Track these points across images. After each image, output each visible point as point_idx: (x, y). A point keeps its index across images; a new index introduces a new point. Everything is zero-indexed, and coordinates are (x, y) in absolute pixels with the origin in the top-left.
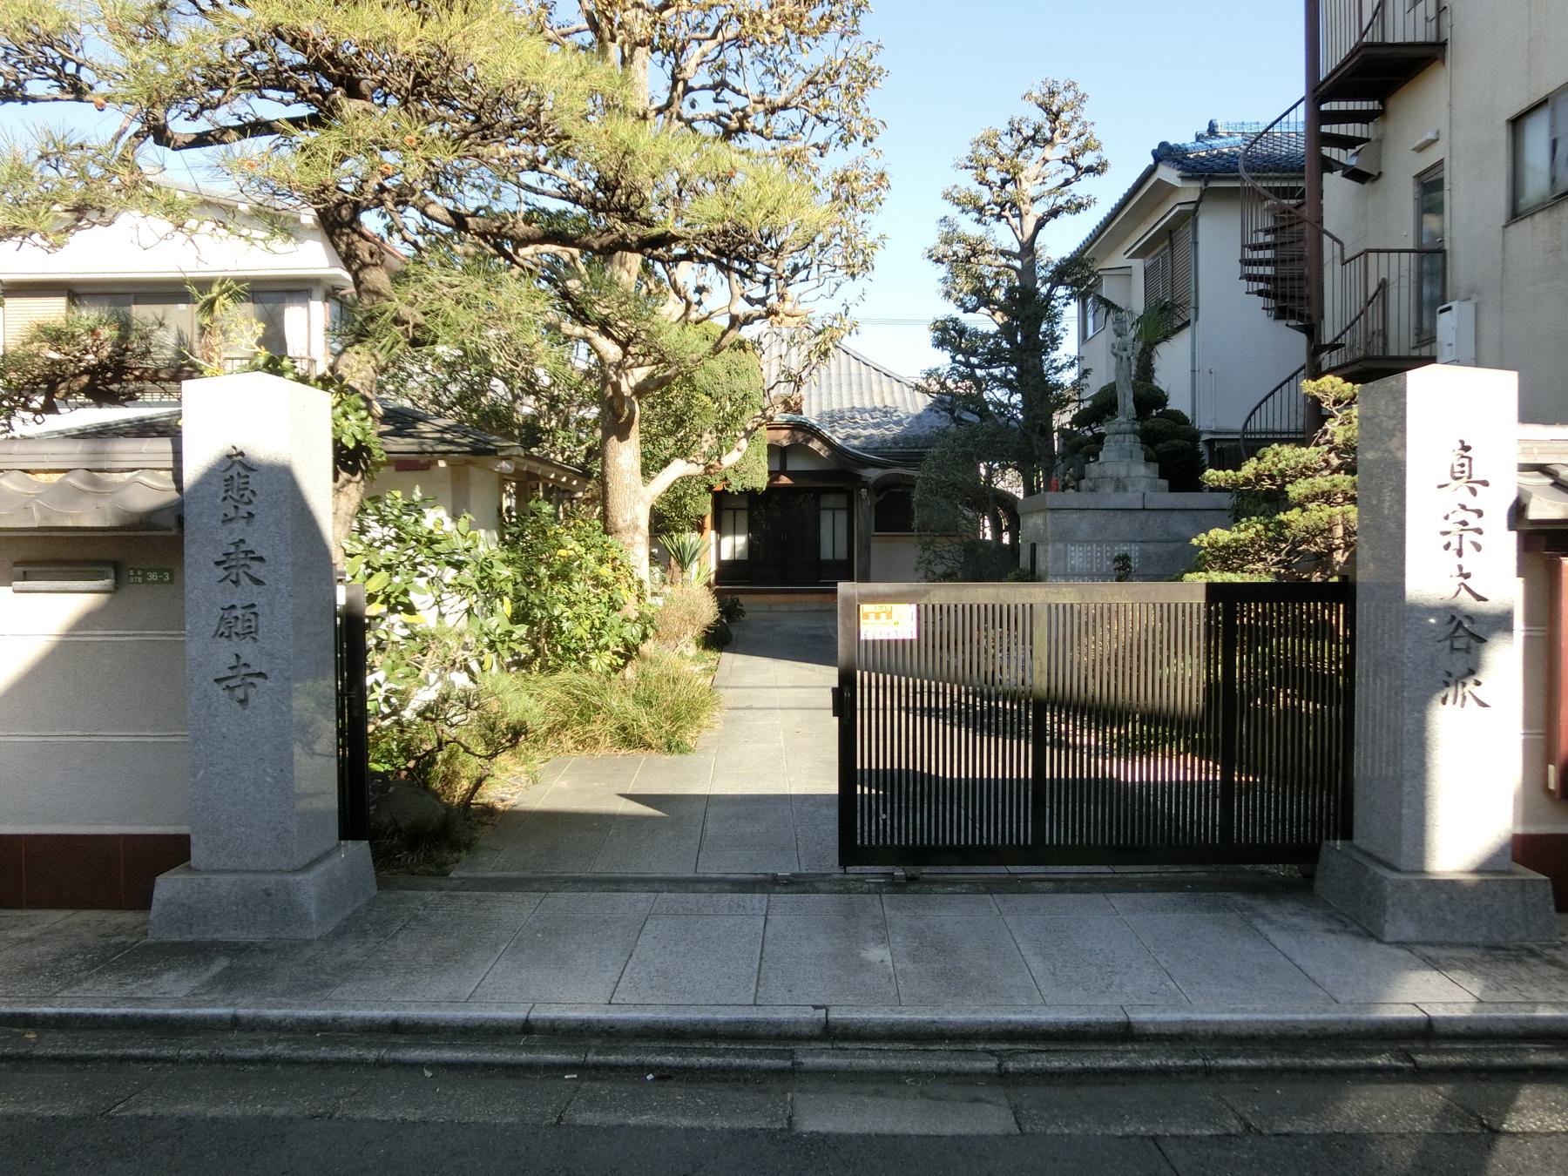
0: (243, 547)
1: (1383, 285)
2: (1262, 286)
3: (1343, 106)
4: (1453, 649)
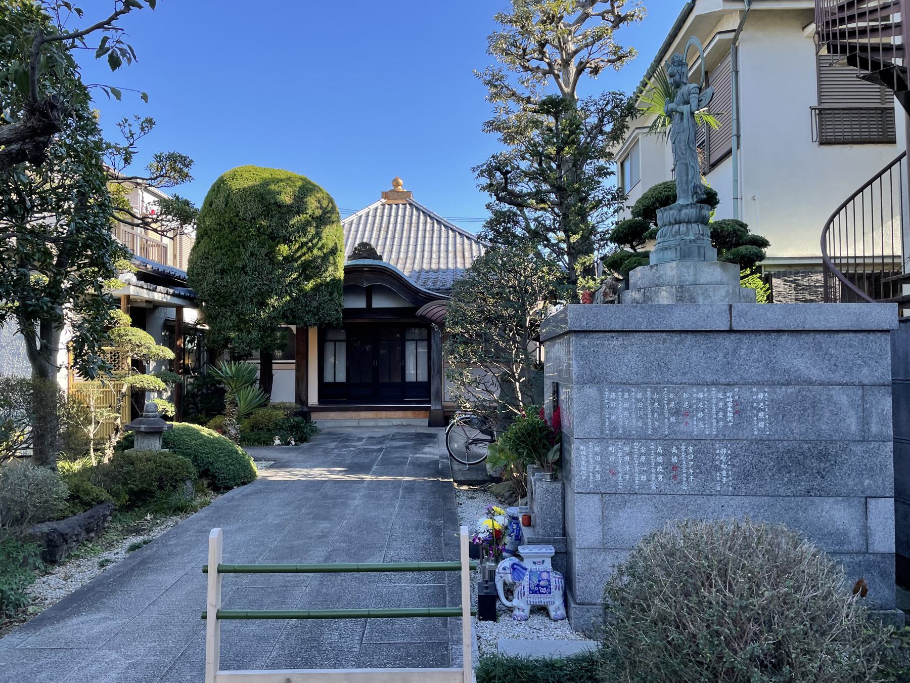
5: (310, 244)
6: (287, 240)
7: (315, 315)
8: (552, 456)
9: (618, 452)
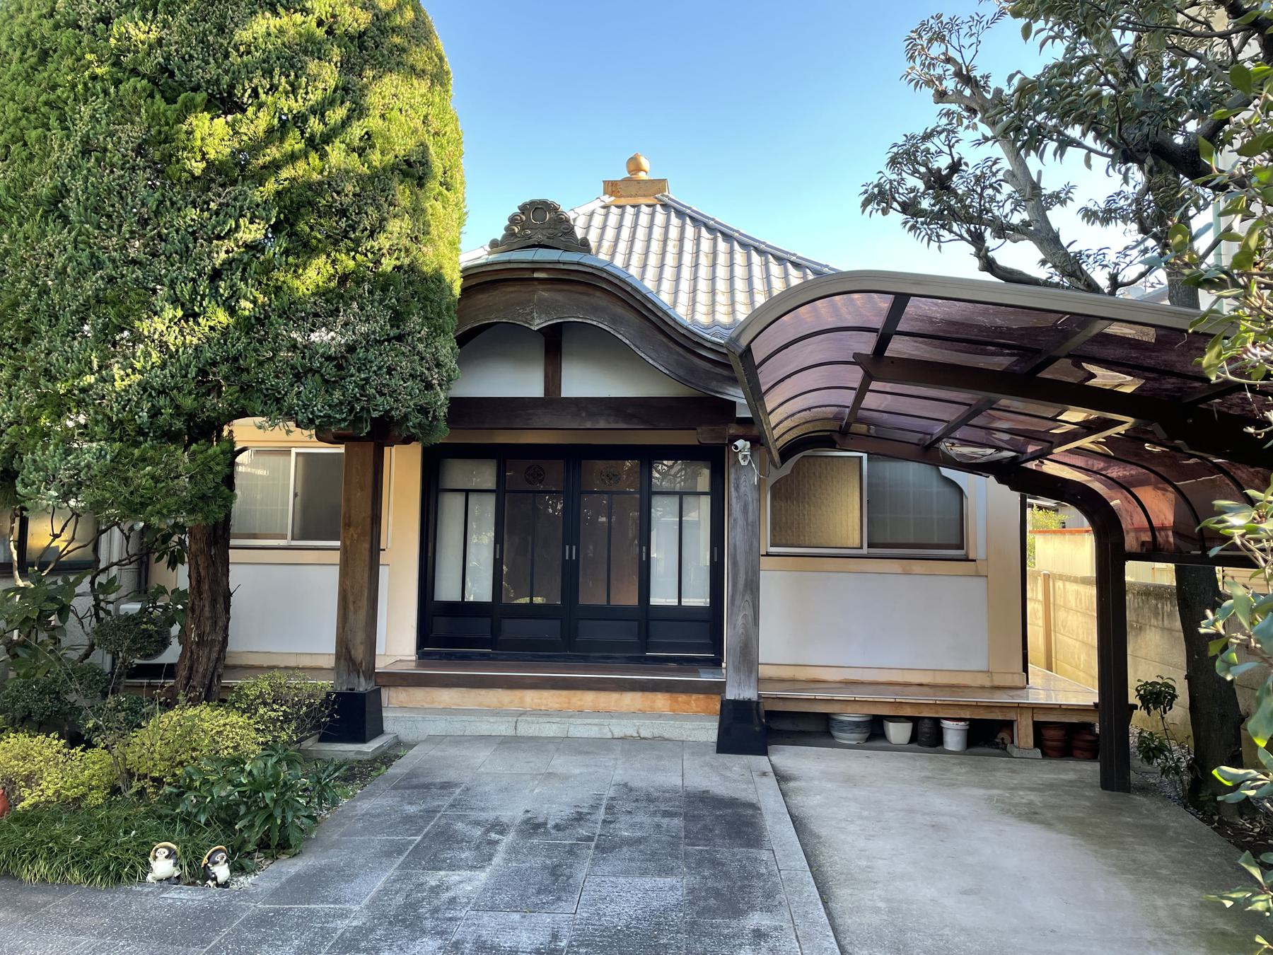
5: (315, 125)
6: (225, 103)
7: (329, 385)
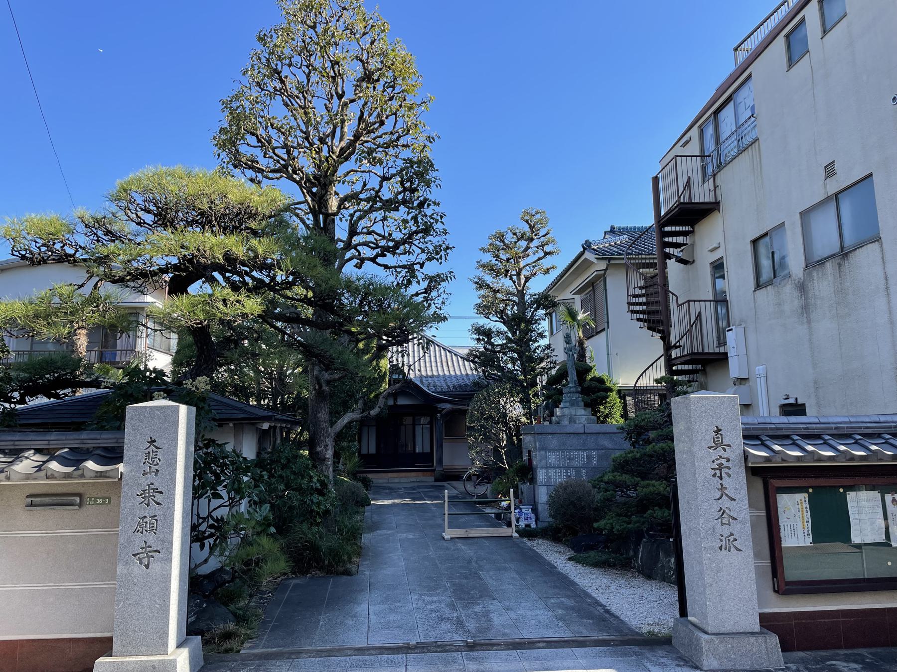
0: (152, 487)
1: (699, 316)
2: (641, 316)
3: (674, 229)
4: (722, 524)
8: (529, 477)
9: (552, 472)
